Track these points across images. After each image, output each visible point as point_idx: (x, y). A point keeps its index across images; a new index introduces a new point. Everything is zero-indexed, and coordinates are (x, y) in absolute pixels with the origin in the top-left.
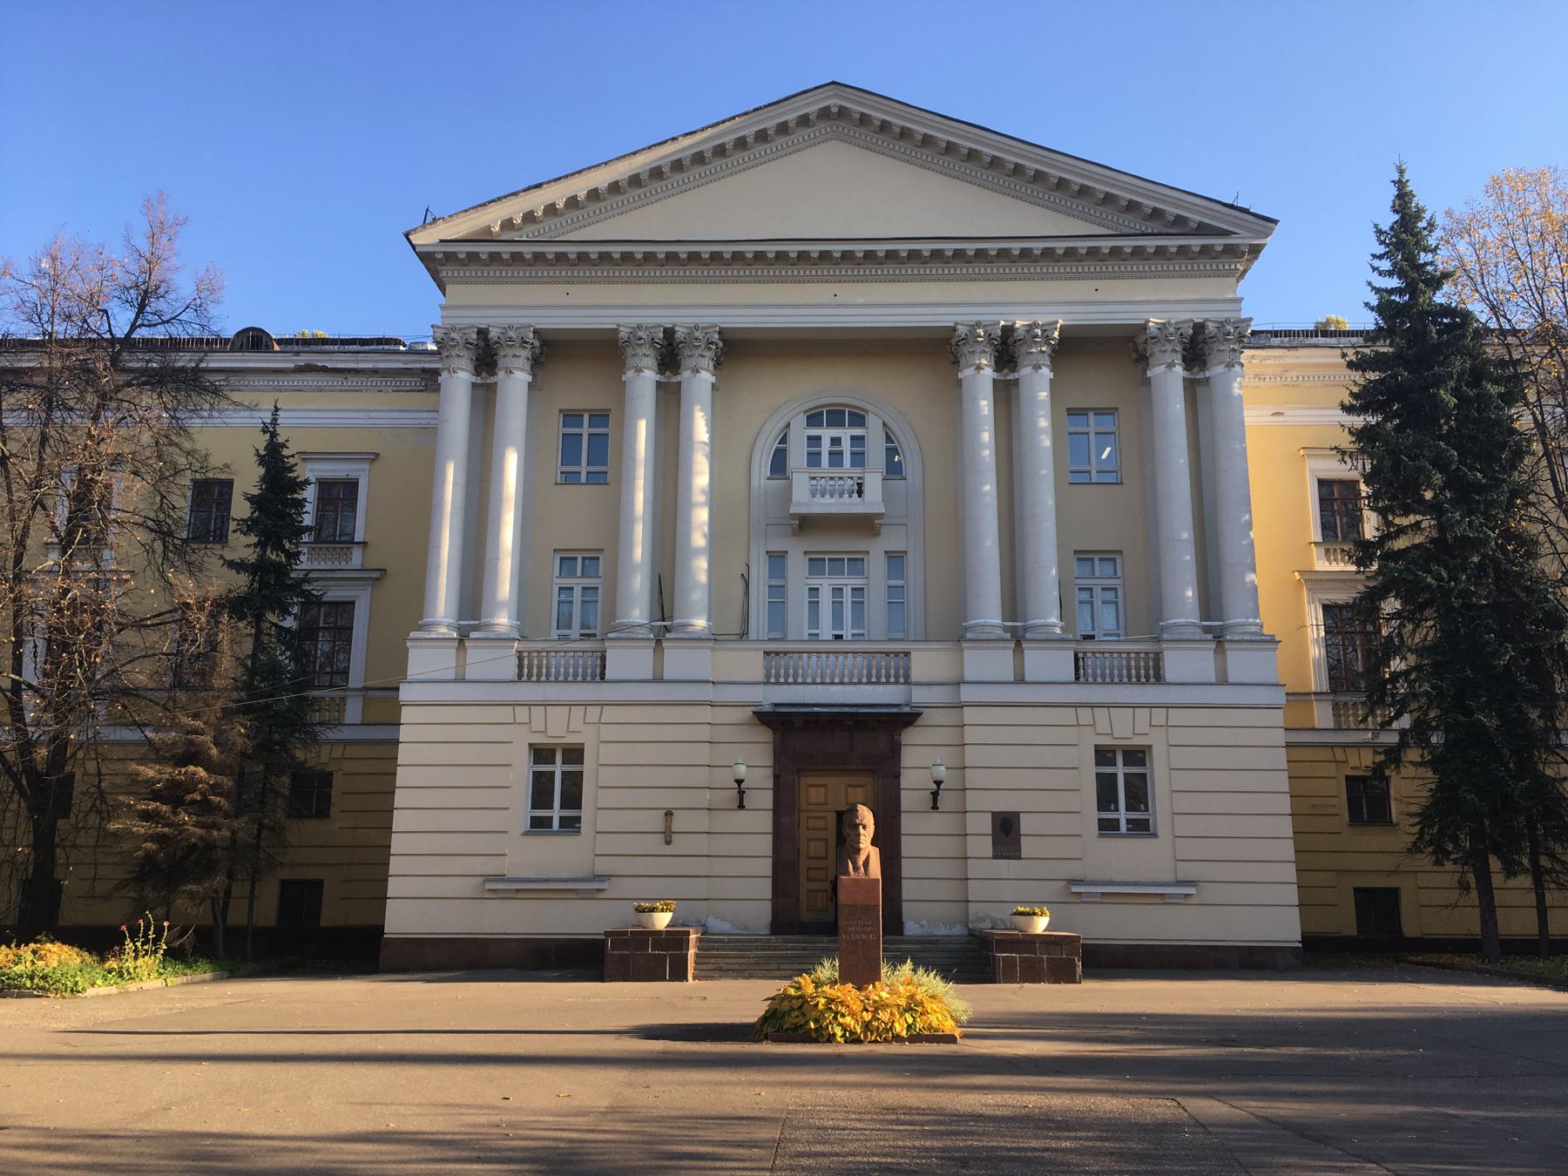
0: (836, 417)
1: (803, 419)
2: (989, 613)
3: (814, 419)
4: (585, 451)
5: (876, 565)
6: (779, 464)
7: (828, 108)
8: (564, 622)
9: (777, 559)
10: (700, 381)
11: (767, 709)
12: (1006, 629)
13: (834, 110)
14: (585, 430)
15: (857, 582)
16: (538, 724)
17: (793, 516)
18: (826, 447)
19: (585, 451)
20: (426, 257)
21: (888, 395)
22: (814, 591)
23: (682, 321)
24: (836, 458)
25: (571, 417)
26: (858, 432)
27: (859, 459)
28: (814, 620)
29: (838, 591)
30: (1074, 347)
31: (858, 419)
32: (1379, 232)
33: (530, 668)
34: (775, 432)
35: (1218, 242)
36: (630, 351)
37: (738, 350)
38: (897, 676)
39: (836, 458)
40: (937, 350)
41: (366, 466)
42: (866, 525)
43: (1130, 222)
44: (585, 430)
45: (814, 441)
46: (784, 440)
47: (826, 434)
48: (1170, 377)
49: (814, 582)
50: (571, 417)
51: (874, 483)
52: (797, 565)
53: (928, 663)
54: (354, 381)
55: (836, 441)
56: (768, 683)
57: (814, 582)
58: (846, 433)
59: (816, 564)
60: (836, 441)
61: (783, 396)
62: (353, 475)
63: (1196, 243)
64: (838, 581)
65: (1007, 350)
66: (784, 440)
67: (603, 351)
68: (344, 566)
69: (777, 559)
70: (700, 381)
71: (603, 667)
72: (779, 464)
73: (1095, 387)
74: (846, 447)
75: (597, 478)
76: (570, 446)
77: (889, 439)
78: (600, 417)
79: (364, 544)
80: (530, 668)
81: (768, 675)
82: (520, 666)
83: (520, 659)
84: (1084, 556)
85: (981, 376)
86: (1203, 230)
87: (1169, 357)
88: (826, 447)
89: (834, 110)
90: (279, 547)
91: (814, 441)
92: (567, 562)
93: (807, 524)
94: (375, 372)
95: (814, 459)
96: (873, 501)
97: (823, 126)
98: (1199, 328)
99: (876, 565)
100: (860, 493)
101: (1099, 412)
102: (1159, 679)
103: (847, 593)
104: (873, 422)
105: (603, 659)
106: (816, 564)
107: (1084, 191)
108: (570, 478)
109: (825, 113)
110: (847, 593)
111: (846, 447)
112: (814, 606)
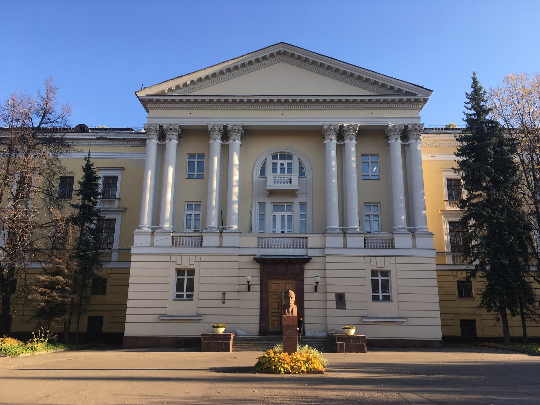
0: (282, 156)
1: (271, 157)
2: (335, 223)
3: (275, 157)
4: (196, 167)
5: (296, 207)
6: (263, 172)
7: (280, 51)
8: (188, 226)
9: (262, 205)
10: (236, 143)
11: (258, 257)
12: (340, 229)
13: (282, 52)
14: (196, 160)
15: (290, 161)
16: (179, 262)
17: (268, 190)
18: (279, 166)
19: (196, 167)
20: (142, 101)
21: (300, 149)
22: (275, 216)
23: (230, 123)
24: (282, 170)
25: (191, 156)
26: (290, 161)
27: (290, 171)
28: (275, 226)
29: (283, 216)
30: (364, 133)
31: (290, 157)
32: (467, 95)
33: (176, 242)
34: (261, 161)
35: (413, 98)
36: (212, 133)
37: (248, 133)
38: (303, 246)
39: (282, 170)
40: (317, 134)
41: (120, 172)
42: (292, 193)
43: (383, 91)
44: (196, 160)
45: (275, 164)
46: (264, 164)
47: (279, 162)
48: (396, 144)
49: (275, 213)
50: (191, 156)
51: (295, 179)
52: (269, 208)
53: (314, 241)
54: (116, 143)
55: (282, 164)
56: (258, 248)
57: (275, 213)
58: (286, 162)
59: (275, 207)
60: (282, 164)
61: (264, 149)
62: (115, 175)
63: (405, 98)
64: (283, 213)
65: (341, 134)
66: (264, 164)
67: (202, 133)
68: (112, 206)
69: (262, 205)
70: (236, 143)
71: (202, 242)
72: (263, 172)
73: (370, 147)
74: (286, 167)
75: (200, 177)
76: (191, 165)
77: (300, 164)
78: (201, 156)
79: (119, 199)
80: (176, 242)
81: (259, 245)
82: (173, 242)
83: (173, 239)
84: (367, 205)
85: (332, 143)
86: (407, 93)
87: (396, 137)
88: (279, 166)
89: (282, 52)
90: (90, 200)
91: (275, 164)
92: (189, 206)
93: (272, 193)
94: (124, 140)
95: (275, 171)
96: (295, 185)
97: (278, 57)
98: (406, 127)
99: (296, 207)
100: (290, 182)
101: (372, 155)
102: (393, 247)
103: (286, 217)
104: (295, 158)
105: (202, 239)
106: (275, 207)
107: (367, 80)
108: (191, 177)
109: (279, 53)
110: (286, 217)
111: (286, 167)
112: (274, 221)
